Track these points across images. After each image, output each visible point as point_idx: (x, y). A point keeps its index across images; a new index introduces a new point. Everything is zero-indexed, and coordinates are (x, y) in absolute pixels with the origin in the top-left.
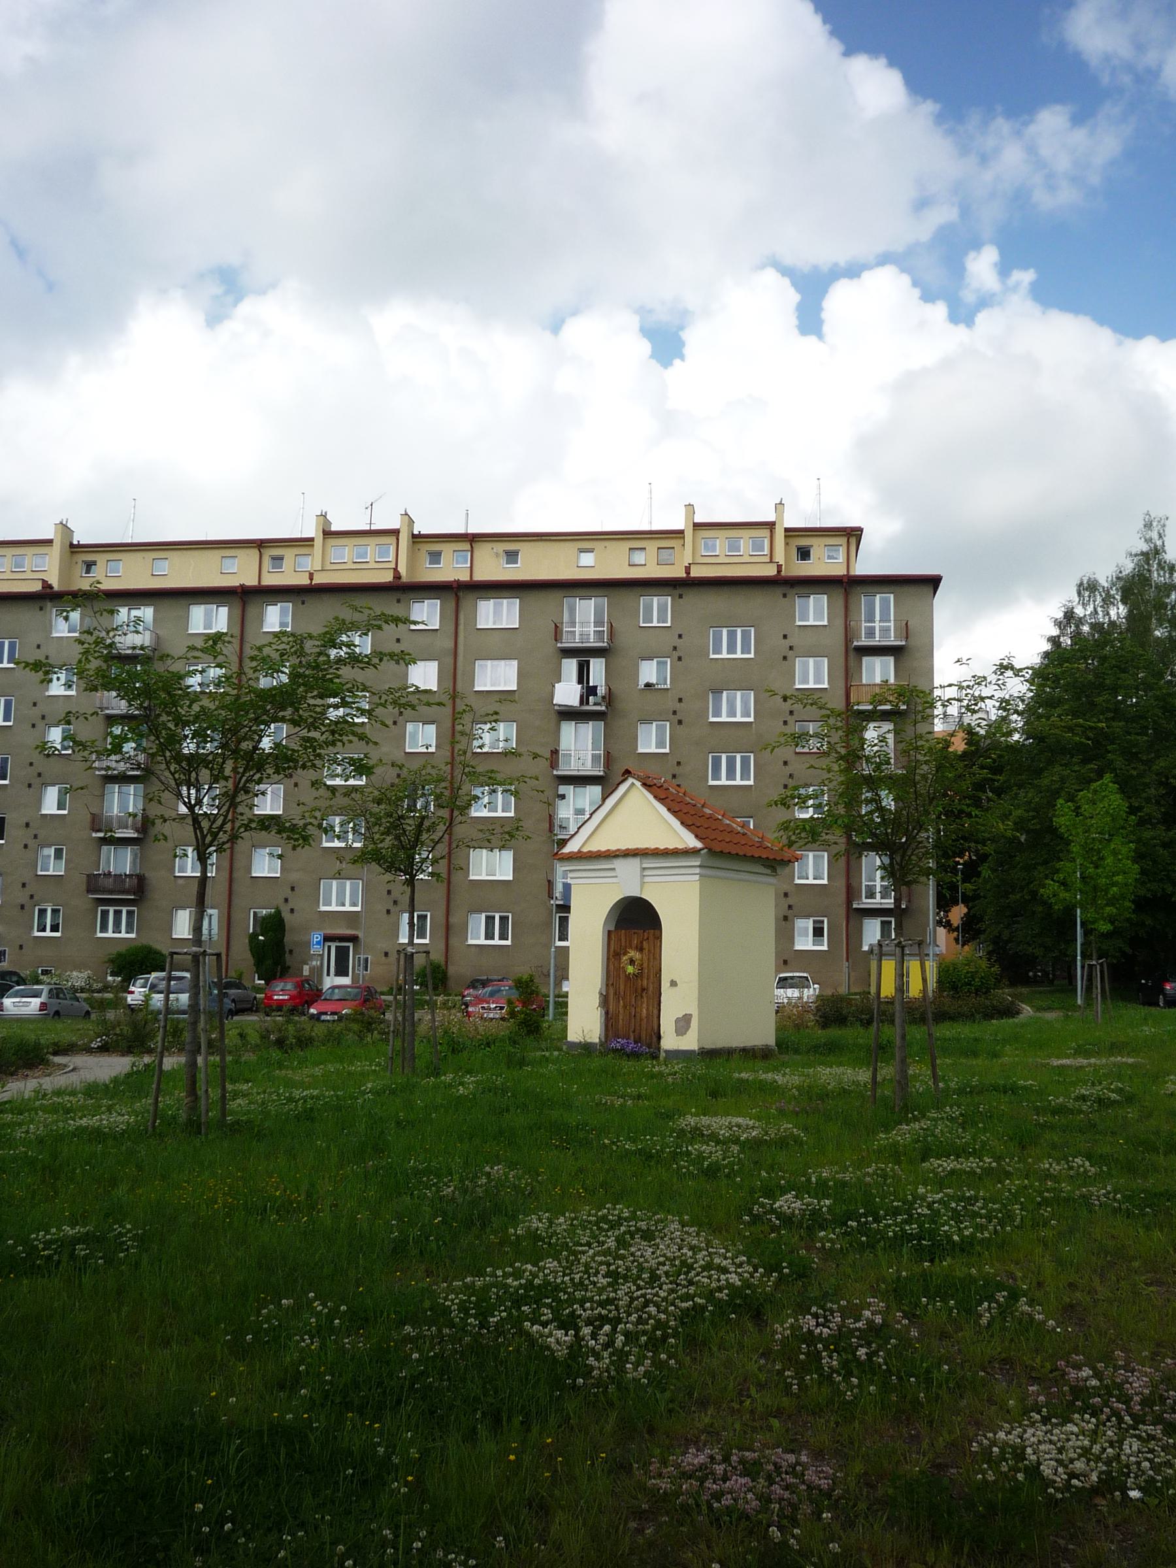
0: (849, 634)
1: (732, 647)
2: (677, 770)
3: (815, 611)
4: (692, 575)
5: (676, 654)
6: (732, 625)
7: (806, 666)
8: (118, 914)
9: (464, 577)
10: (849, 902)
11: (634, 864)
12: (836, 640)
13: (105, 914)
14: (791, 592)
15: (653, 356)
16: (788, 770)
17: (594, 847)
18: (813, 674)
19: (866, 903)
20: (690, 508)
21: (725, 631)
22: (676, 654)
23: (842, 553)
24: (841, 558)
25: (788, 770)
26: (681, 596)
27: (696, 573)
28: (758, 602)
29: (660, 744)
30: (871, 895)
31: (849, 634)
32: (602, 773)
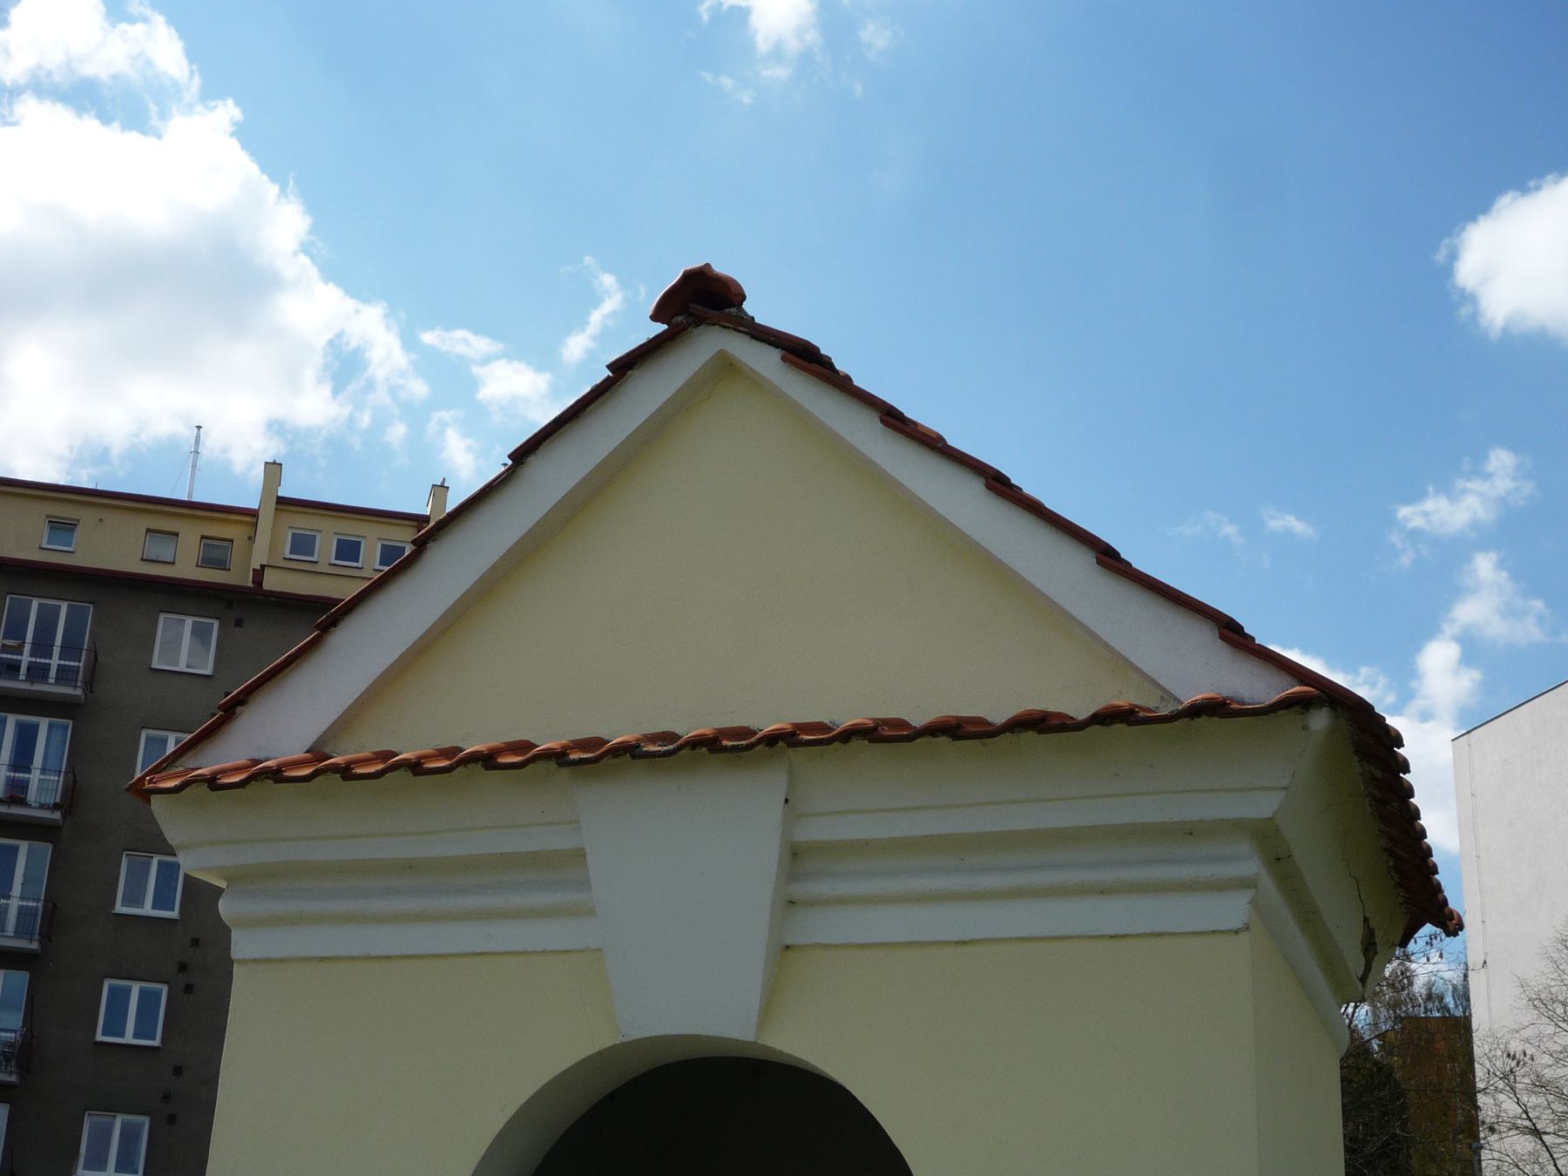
4: (267, 586)
20: (273, 469)
26: (239, 623)
27: (272, 582)
29: (162, 901)
32: (35, 946)
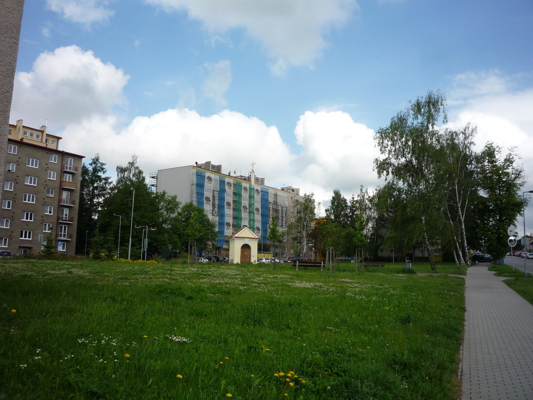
0: (62, 167)
1: (33, 165)
2: (15, 197)
3: (54, 160)
5: (18, 163)
6: (33, 158)
7: (66, 176)
8: (65, 227)
9: (55, 148)
10: (56, 238)
11: (248, 239)
12: (59, 168)
13: (62, 227)
14: (50, 153)
15: (150, 117)
16: (44, 201)
17: (240, 236)
18: (53, 177)
19: (60, 238)
21: (31, 159)
22: (18, 163)
23: (56, 143)
24: (55, 145)
25: (44, 201)
27: (24, 141)
28: (40, 153)
30: (61, 236)
31: (62, 167)
